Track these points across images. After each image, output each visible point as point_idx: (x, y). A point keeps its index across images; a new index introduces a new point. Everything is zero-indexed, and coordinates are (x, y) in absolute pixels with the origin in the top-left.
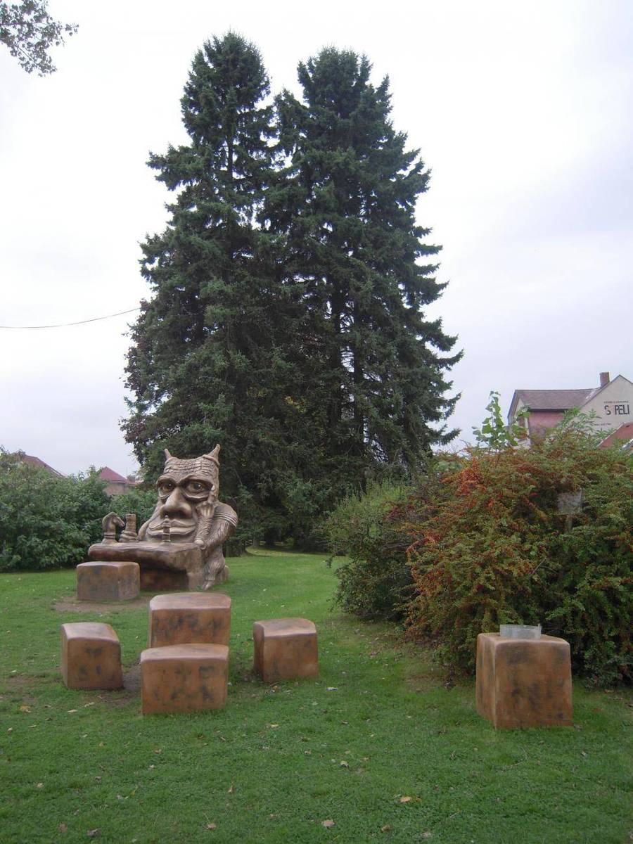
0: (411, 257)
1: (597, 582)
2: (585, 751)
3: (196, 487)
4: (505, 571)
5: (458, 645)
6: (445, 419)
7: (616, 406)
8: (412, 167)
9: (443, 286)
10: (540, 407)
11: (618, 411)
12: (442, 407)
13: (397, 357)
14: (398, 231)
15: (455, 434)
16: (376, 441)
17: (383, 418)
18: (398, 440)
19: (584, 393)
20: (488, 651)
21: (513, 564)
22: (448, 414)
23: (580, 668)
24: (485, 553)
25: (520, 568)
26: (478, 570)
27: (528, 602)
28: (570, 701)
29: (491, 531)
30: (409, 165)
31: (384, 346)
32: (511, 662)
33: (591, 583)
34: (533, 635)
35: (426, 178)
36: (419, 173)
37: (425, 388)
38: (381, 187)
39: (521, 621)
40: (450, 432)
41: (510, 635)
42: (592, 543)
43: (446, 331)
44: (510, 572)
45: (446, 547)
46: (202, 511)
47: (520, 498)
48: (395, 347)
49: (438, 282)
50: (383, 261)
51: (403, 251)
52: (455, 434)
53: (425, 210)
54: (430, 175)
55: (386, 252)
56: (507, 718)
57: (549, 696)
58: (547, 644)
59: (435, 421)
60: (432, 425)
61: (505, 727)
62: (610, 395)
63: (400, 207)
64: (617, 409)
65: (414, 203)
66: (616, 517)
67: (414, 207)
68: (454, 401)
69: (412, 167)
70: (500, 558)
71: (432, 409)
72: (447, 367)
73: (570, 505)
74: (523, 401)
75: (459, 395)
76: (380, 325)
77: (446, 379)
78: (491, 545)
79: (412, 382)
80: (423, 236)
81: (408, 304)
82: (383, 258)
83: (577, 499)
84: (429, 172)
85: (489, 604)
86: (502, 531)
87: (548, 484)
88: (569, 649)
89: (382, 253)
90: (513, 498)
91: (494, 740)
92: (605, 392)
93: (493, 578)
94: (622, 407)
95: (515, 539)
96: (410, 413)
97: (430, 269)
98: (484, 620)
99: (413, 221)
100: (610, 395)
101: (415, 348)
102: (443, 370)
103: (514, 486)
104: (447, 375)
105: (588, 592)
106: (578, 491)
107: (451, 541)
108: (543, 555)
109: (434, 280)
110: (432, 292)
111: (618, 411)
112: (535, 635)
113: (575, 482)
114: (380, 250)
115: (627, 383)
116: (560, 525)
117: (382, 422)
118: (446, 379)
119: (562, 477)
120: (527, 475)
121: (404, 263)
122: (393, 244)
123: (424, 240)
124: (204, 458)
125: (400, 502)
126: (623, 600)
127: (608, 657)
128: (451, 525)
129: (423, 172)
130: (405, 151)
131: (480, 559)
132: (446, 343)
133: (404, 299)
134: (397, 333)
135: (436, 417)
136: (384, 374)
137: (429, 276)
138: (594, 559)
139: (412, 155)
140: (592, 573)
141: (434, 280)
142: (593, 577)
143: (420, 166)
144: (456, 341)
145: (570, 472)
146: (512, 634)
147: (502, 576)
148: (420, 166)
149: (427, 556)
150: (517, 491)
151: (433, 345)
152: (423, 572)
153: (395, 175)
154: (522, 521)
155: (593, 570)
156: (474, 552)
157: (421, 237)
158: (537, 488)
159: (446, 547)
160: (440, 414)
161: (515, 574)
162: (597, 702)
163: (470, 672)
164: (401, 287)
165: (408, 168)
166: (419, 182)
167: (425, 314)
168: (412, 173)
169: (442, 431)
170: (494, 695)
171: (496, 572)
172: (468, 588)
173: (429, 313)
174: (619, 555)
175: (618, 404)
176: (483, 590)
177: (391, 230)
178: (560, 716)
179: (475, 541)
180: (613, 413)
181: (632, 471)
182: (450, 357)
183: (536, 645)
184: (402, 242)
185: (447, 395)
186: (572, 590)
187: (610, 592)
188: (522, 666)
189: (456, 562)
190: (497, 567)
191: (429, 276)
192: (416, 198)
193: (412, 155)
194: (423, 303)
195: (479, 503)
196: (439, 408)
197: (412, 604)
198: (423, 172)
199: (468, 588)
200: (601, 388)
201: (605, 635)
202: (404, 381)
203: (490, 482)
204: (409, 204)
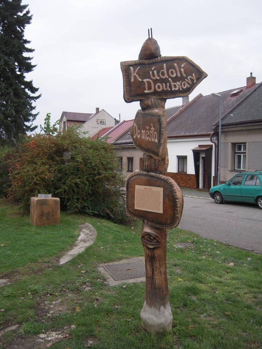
0: (21, 52)
1: (73, 181)
2: (62, 230)
4: (43, 177)
5: (26, 203)
6: (32, 121)
8: (24, 12)
9: (34, 66)
10: (74, 120)
12: (31, 117)
13: (13, 94)
14: (16, 40)
15: (36, 127)
16: (2, 129)
17: (5, 119)
18: (12, 129)
19: (89, 115)
20: (34, 202)
21: (46, 175)
22: (33, 120)
23: (64, 208)
24: (37, 171)
25: (48, 176)
26: (34, 177)
27: (50, 188)
28: (59, 217)
29: (39, 164)
30: (23, 11)
31: (7, 89)
32: (41, 205)
33: (70, 181)
34: (49, 197)
35: (30, 18)
36: (27, 15)
37: (25, 108)
38: (10, 19)
39: (48, 193)
40: (34, 127)
41: (41, 197)
42: (72, 168)
43: (35, 85)
44: (45, 178)
45: (23, 169)
47: (50, 153)
48: (12, 91)
49: (32, 64)
50: (9, 52)
51: (18, 49)
52: (36, 127)
53: (29, 32)
54: (32, 17)
55: (10, 49)
56: (39, 223)
57: (53, 215)
58: (53, 199)
59: (28, 122)
60: (27, 123)
61: (38, 226)
62: (100, 117)
63: (18, 29)
64: (101, 122)
65: (24, 28)
66: (80, 160)
67: (24, 30)
68: (36, 115)
69: (24, 12)
70: (42, 173)
71: (27, 117)
72: (34, 100)
73: (67, 156)
74: (66, 117)
75: (39, 113)
76: (6, 80)
77: (33, 105)
78: (39, 169)
79: (19, 105)
80: (27, 43)
81: (19, 71)
82: (9, 51)
83: (70, 153)
84: (32, 16)
85: (37, 188)
86: (44, 164)
87: (60, 148)
88: (60, 201)
89: (9, 49)
90: (48, 153)
91: (34, 230)
92: (97, 115)
93: (39, 179)
94: (103, 122)
95: (47, 166)
96: (17, 118)
97: (29, 59)
98: (36, 193)
99: (23, 36)
100: (100, 117)
101: (21, 92)
102: (32, 101)
103: (48, 149)
104: (34, 104)
105: (70, 184)
106: (70, 151)
107: (25, 167)
108: (56, 172)
109: (31, 63)
110: (29, 68)
112: (49, 197)
113: (70, 147)
114: (8, 47)
115: (106, 113)
116: (63, 162)
117: (5, 121)
118: (33, 105)
119: (64, 146)
120: (53, 145)
121: (18, 55)
122: (14, 45)
123: (27, 46)
125: (8, 153)
126: (80, 186)
127: (75, 204)
128: (26, 161)
129: (29, 15)
130: (22, 4)
131: (35, 173)
132: (34, 90)
133: (17, 70)
134: (13, 84)
135: (28, 120)
136: (7, 101)
137: (29, 61)
138: (72, 173)
139: (25, 7)
140: (71, 178)
141: (31, 63)
142: (71, 179)
143: (28, 12)
144: (39, 90)
145: (68, 145)
146: (42, 197)
147: (42, 179)
148: (28, 12)
149: (16, 172)
150: (49, 150)
151: (29, 91)
152: (14, 178)
153: (16, 15)
154: (50, 161)
155: (71, 177)
156: (33, 171)
157: (26, 44)
158: (56, 150)
159: (23, 169)
160: (30, 119)
161: (46, 178)
162: (70, 218)
163: (28, 212)
164: (16, 64)
165: (23, 12)
166: (27, 19)
167: (26, 77)
168: (25, 15)
169: (31, 126)
170: (35, 216)
171: (40, 178)
172: (30, 183)
173: (28, 77)
174: (80, 172)
175: (102, 120)
176: (36, 184)
177: (13, 39)
178: (56, 222)
179: (33, 167)
180: (99, 123)
181: (248, 165)
182: (36, 96)
183: (49, 199)
184: (18, 45)
185: (34, 112)
186: (64, 184)
187: (76, 184)
188: (44, 206)
189: (26, 174)
190: (40, 176)
191: (29, 61)
192: (25, 26)
193: (25, 7)
194: (25, 72)
195: (36, 154)
196: (30, 117)
197: (10, 189)
198: (29, 15)
199: (30, 183)
200: (96, 114)
201: (74, 198)
202: (15, 105)
203: (41, 147)
204: (22, 28)
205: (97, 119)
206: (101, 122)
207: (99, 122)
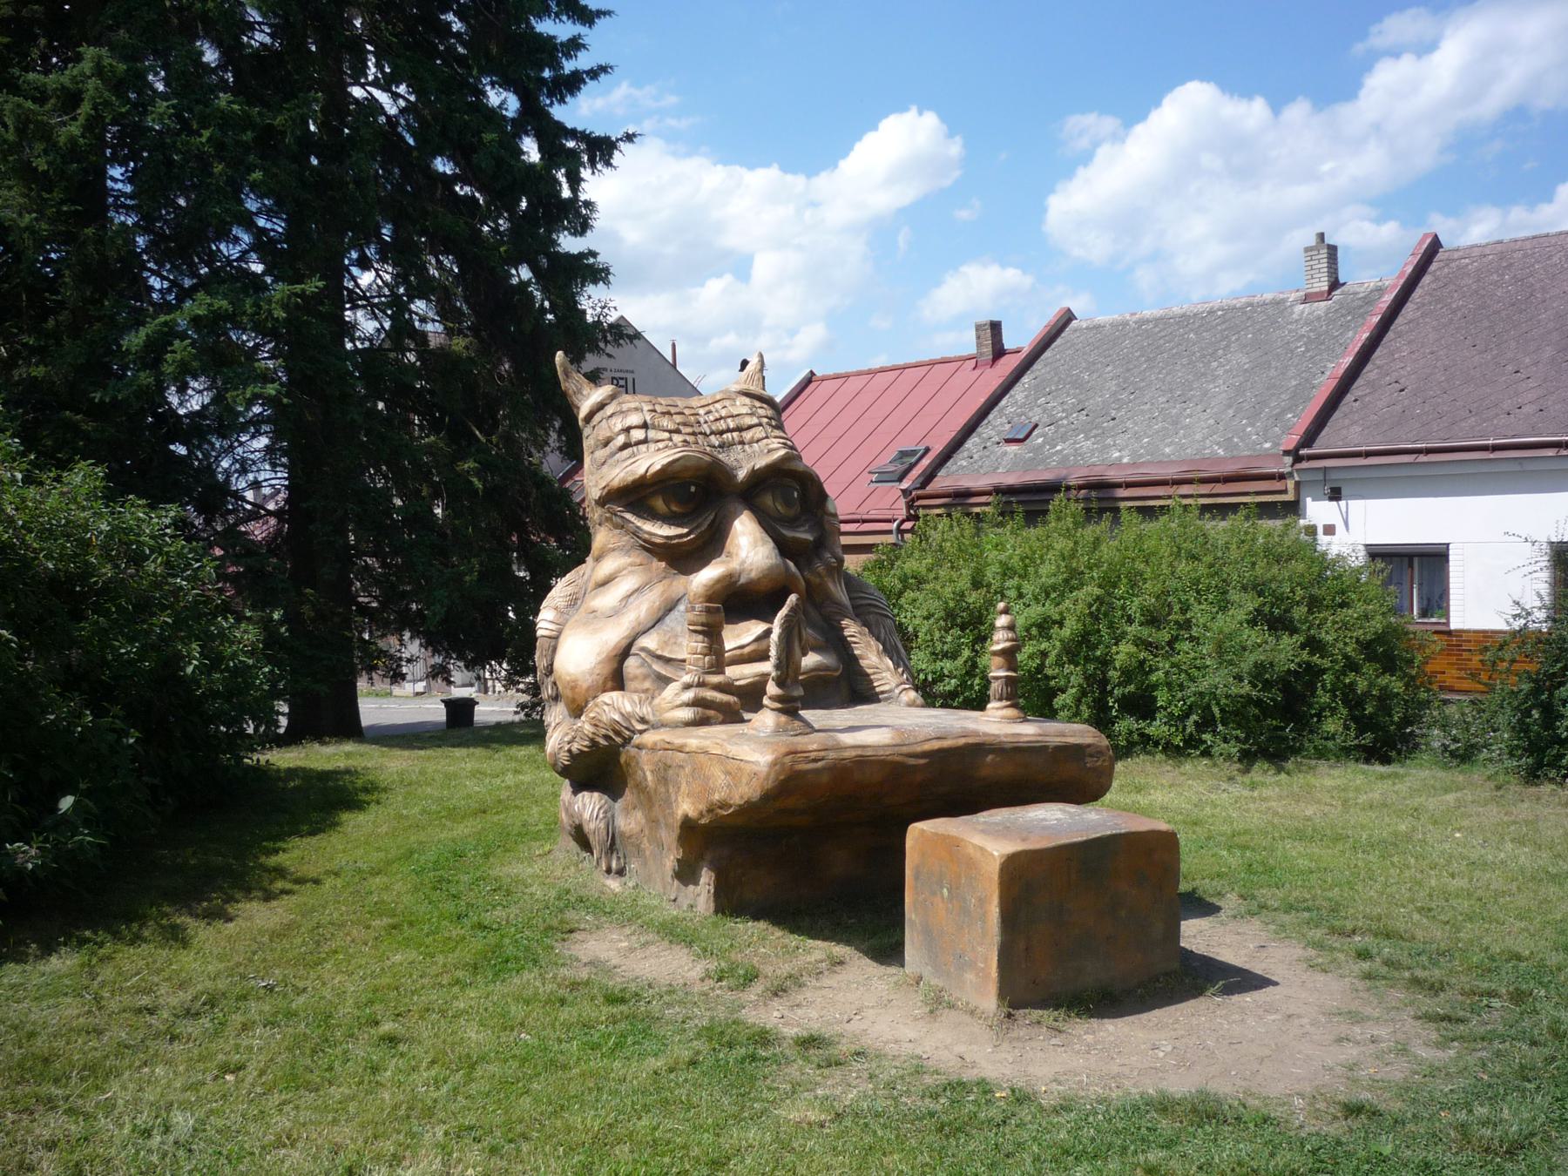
3: (788, 503)
46: (831, 585)
175: (618, 375)
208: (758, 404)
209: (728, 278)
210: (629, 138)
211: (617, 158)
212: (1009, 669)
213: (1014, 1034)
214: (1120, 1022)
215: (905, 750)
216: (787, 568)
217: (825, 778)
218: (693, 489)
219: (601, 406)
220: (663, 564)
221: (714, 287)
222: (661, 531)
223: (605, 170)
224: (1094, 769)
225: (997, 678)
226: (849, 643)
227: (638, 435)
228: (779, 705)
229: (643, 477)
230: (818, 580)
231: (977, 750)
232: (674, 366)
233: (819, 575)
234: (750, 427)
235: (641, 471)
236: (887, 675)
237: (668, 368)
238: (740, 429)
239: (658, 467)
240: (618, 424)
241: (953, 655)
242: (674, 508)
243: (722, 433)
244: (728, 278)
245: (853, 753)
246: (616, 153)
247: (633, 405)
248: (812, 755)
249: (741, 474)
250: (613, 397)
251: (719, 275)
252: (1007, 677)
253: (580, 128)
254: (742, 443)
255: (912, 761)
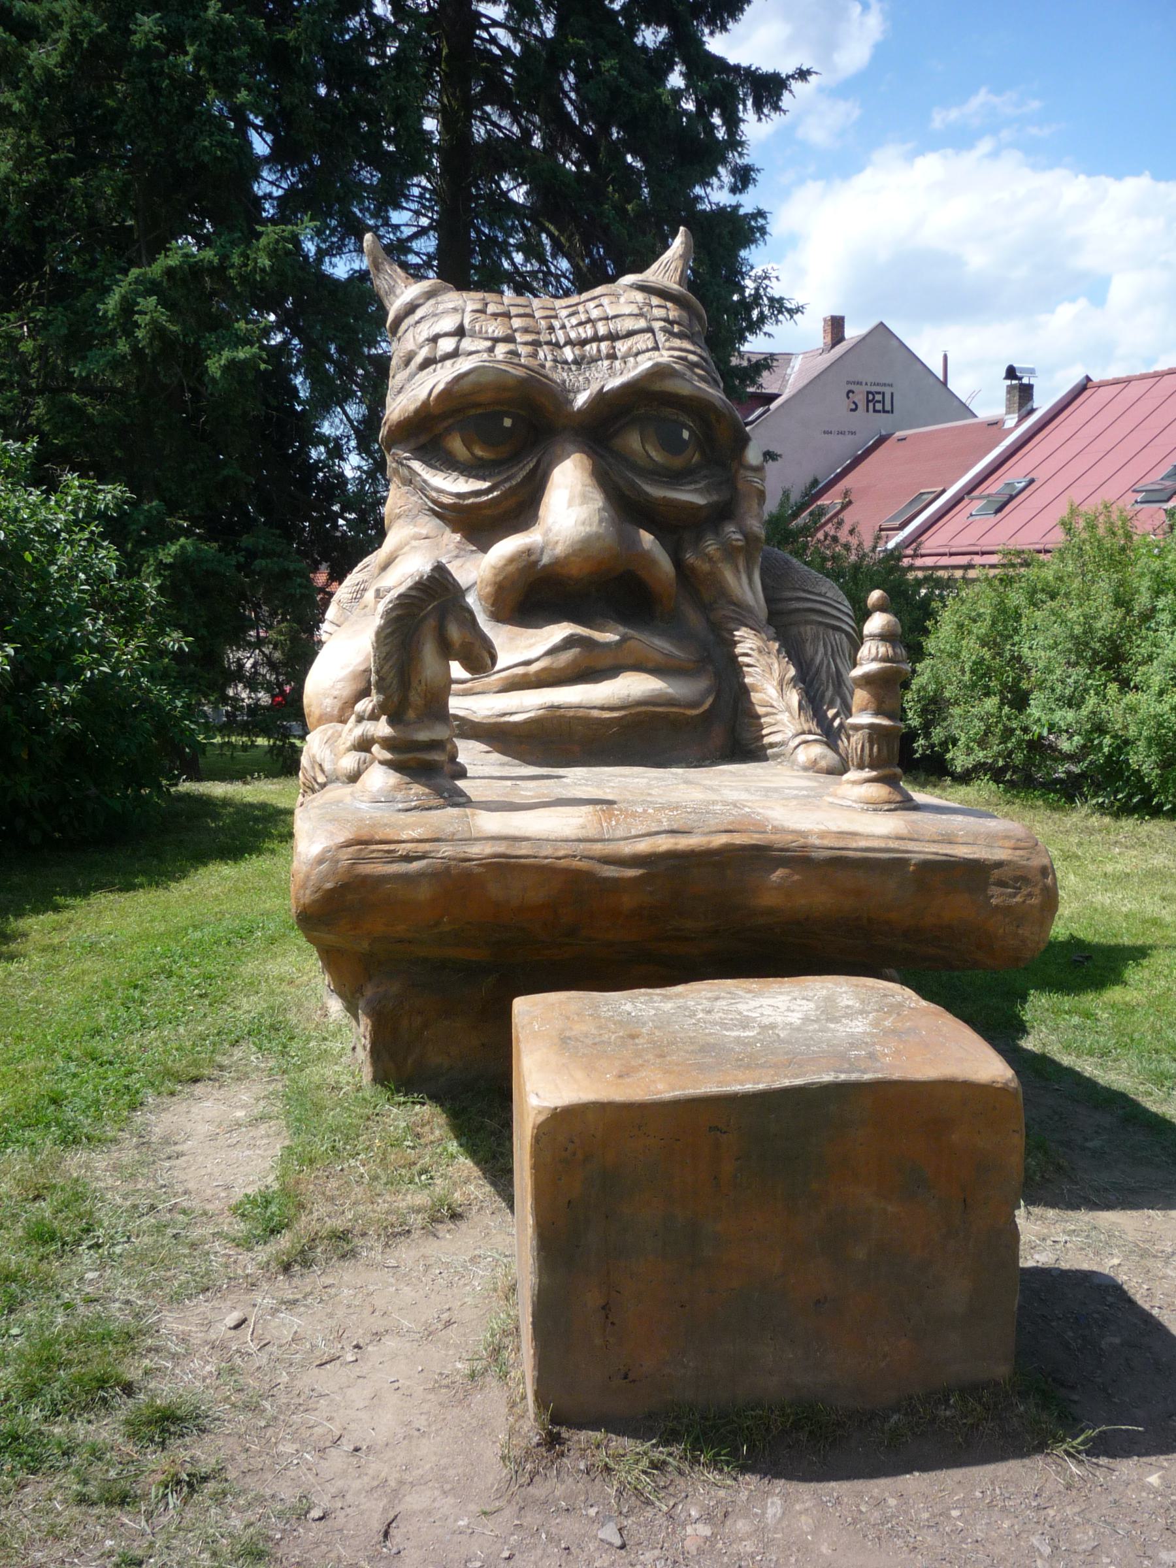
3: (672, 445)
7: (868, 393)
11: (871, 405)
46: (729, 576)
111: (871, 405)
124: (643, 288)
175: (874, 389)
205: (848, 383)
206: (868, 401)
207: (860, 398)
208: (655, 301)
209: (1082, 303)
210: (803, 75)
211: (786, 100)
212: (878, 712)
213: (538, 1490)
214: (806, 1494)
215: (598, 849)
216: (630, 544)
217: (424, 893)
218: (508, 422)
219: (411, 308)
220: (457, 537)
221: (1066, 312)
222: (452, 485)
223: (773, 115)
224: (1007, 910)
225: (857, 728)
226: (742, 671)
227: (446, 345)
228: (388, 756)
229: (426, 404)
230: (706, 567)
231: (751, 859)
232: (945, 383)
233: (711, 560)
234: (630, 334)
235: (423, 395)
236: (784, 717)
237: (941, 386)
238: (613, 337)
239: (441, 386)
240: (425, 331)
241: (1073, 702)
242: (479, 452)
243: (583, 343)
244: (1082, 303)
245: (488, 849)
246: (786, 94)
247: (451, 305)
248: (402, 849)
249: (581, 400)
250: (430, 295)
251: (1073, 300)
252: (871, 726)
253: (744, 64)
254: (612, 357)
255: (611, 872)
